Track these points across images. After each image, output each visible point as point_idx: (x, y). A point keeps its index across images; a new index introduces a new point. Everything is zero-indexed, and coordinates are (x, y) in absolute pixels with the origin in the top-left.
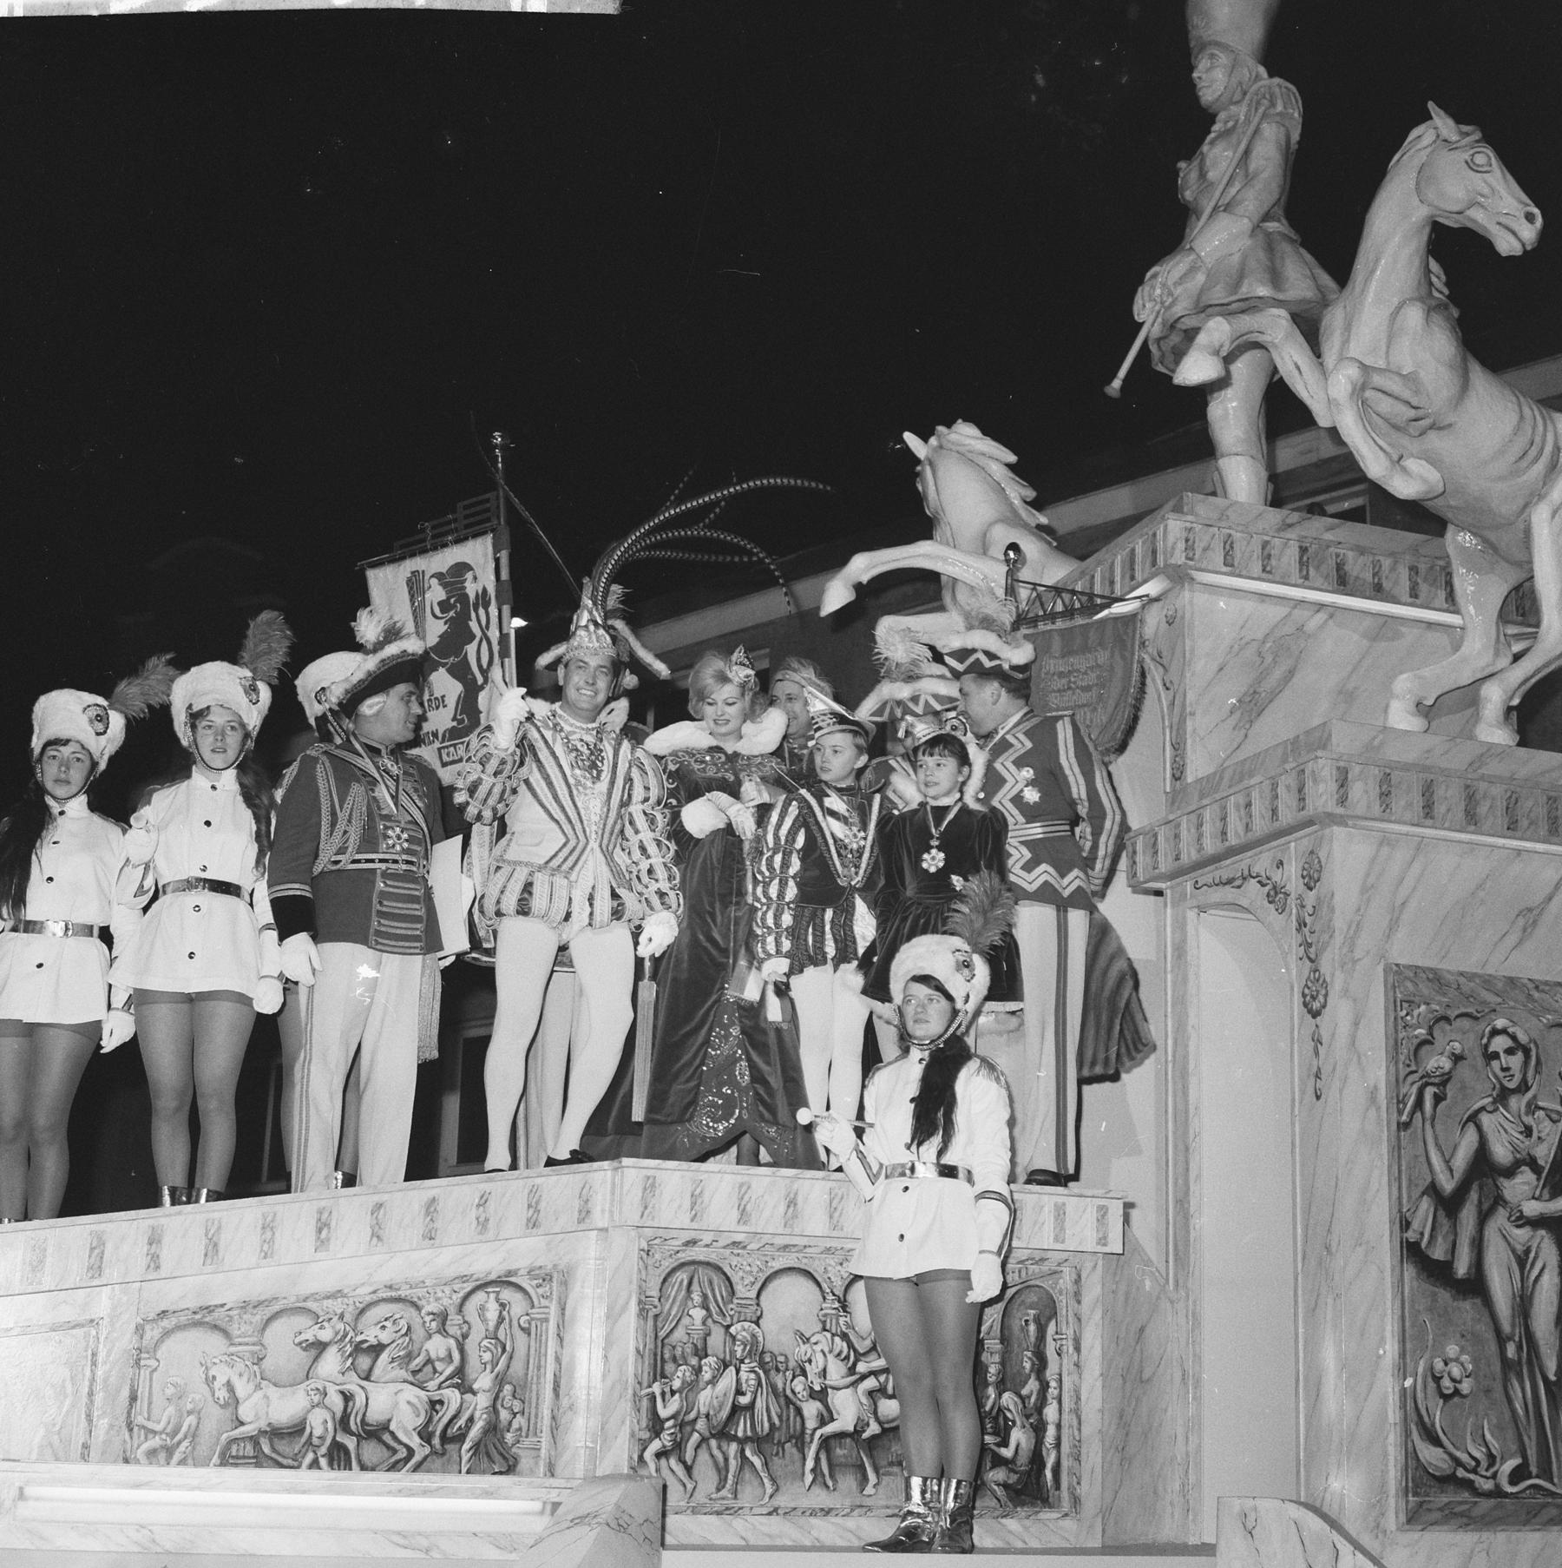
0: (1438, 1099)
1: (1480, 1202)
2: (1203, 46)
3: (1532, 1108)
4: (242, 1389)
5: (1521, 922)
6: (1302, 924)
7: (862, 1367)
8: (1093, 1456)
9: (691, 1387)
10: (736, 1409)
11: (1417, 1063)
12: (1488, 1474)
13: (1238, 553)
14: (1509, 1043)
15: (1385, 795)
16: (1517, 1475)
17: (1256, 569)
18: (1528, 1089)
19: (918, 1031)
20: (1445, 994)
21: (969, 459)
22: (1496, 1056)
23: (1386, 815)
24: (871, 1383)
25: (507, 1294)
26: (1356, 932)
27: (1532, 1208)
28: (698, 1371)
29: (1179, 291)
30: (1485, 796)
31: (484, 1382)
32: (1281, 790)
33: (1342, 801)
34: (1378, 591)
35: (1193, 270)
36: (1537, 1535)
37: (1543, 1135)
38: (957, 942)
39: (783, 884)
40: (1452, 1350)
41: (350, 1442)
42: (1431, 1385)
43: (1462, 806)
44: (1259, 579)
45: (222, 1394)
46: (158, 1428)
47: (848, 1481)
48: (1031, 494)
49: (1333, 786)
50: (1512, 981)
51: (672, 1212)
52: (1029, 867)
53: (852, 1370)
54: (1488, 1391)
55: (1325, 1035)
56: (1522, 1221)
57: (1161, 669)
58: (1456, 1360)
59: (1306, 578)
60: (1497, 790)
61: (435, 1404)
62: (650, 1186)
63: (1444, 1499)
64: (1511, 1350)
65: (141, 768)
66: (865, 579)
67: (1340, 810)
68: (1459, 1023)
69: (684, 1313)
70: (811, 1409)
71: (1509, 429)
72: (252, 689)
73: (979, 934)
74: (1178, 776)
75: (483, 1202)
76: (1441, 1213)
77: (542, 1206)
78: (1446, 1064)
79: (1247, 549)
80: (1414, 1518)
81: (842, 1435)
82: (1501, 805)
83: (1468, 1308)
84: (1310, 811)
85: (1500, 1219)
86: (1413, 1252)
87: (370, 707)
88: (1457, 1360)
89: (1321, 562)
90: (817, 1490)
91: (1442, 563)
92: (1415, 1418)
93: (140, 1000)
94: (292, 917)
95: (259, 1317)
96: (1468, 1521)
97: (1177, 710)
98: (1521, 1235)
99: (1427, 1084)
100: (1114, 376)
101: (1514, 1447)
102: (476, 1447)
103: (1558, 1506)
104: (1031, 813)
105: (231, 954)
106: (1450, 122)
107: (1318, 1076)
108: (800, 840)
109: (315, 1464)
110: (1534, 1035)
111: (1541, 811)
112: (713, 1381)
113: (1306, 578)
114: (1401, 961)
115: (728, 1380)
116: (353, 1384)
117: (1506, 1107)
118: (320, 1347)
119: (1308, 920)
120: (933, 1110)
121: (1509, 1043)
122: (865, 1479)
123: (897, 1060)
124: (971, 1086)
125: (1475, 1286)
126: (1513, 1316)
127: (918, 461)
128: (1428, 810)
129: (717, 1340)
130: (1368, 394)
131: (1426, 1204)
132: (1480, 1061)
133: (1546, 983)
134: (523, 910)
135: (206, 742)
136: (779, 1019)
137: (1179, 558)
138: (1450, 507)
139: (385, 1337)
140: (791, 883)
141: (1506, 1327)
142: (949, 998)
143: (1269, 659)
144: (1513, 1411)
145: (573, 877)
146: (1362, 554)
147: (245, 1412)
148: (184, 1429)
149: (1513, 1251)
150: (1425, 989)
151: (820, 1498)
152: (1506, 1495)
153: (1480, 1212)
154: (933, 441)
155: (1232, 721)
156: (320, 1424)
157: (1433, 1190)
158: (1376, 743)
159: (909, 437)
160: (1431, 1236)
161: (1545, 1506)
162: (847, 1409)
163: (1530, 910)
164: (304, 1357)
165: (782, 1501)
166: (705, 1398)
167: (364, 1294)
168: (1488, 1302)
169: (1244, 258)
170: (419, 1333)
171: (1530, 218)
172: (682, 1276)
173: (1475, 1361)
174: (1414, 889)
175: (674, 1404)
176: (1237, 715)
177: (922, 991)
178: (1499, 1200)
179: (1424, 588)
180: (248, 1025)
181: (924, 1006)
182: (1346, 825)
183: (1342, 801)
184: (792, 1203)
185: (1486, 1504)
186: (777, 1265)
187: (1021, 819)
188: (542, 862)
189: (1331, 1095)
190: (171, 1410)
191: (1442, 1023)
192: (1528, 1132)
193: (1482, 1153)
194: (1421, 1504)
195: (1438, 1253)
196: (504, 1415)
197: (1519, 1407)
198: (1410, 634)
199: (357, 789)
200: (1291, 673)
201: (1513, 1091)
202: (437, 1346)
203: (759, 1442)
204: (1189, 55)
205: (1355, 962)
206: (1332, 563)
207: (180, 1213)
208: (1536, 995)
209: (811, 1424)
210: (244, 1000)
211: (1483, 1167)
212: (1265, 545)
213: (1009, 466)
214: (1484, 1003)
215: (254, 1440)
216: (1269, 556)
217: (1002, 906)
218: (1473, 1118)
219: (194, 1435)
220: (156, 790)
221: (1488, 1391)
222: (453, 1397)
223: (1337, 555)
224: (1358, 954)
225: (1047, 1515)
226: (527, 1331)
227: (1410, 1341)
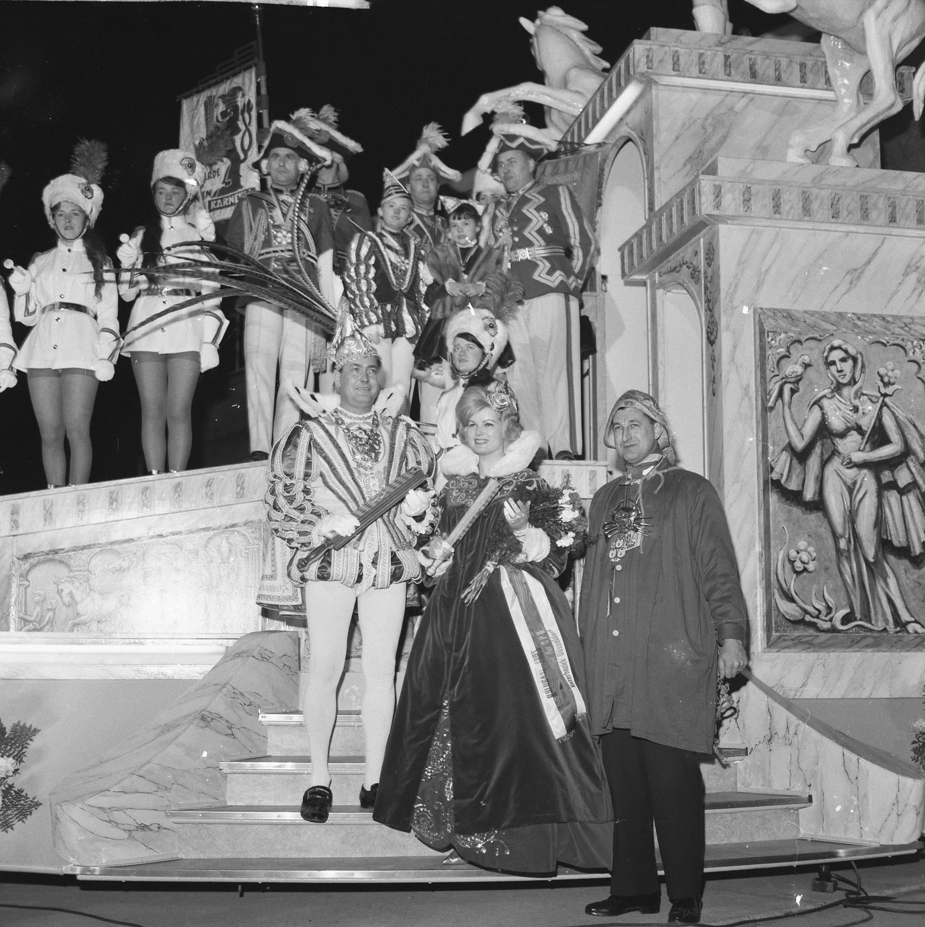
0: (793, 392)
1: (822, 454)
3: (859, 394)
5: (849, 278)
6: (706, 288)
11: (779, 370)
12: (827, 619)
14: (842, 354)
15: (747, 201)
16: (846, 619)
17: (695, 71)
18: (855, 383)
19: (462, 367)
20: (797, 326)
22: (834, 363)
23: (748, 214)
26: (734, 291)
27: (858, 457)
30: (816, 198)
33: (718, 206)
36: (859, 654)
37: (866, 411)
38: (486, 313)
40: (802, 544)
42: (788, 566)
43: (801, 204)
44: (698, 78)
45: (67, 599)
46: (32, 619)
48: (599, 49)
49: (712, 197)
50: (841, 315)
52: (550, 273)
54: (826, 569)
56: (851, 465)
58: (805, 550)
59: (729, 75)
63: (796, 634)
64: (843, 544)
67: (716, 212)
72: (87, 191)
74: (651, 209)
75: (209, 484)
76: (795, 461)
77: (245, 485)
78: (799, 369)
82: (827, 203)
83: (814, 518)
86: (773, 485)
88: (805, 551)
89: (740, 64)
91: (822, 59)
92: (777, 586)
96: (809, 645)
98: (851, 473)
99: (786, 382)
101: (845, 603)
103: (874, 637)
110: (861, 349)
111: (855, 205)
113: (729, 75)
114: (764, 306)
117: (840, 395)
121: (842, 354)
125: (819, 505)
126: (845, 524)
127: (529, 36)
128: (777, 208)
131: (785, 457)
132: (822, 367)
133: (864, 315)
138: (812, 18)
140: (373, 282)
141: (839, 529)
142: (480, 346)
143: (710, 130)
144: (844, 580)
146: (767, 57)
148: (47, 619)
149: (845, 483)
150: (783, 324)
152: (840, 631)
153: (822, 460)
154: (538, 22)
157: (790, 447)
158: (748, 170)
159: (524, 22)
160: (788, 476)
161: (865, 637)
163: (855, 270)
173: (818, 551)
174: (774, 261)
176: (688, 166)
177: (463, 342)
178: (835, 452)
179: (810, 77)
180: (94, 389)
182: (727, 223)
183: (718, 206)
185: (823, 637)
190: (38, 609)
191: (796, 344)
192: (856, 409)
194: (780, 637)
195: (793, 486)
200: (725, 138)
201: (845, 385)
206: (747, 64)
207: (28, 497)
208: (859, 323)
210: (91, 373)
211: (823, 431)
212: (701, 55)
213: (584, 33)
214: (824, 330)
216: (704, 63)
217: (512, 290)
220: (37, 256)
221: (826, 569)
223: (750, 59)
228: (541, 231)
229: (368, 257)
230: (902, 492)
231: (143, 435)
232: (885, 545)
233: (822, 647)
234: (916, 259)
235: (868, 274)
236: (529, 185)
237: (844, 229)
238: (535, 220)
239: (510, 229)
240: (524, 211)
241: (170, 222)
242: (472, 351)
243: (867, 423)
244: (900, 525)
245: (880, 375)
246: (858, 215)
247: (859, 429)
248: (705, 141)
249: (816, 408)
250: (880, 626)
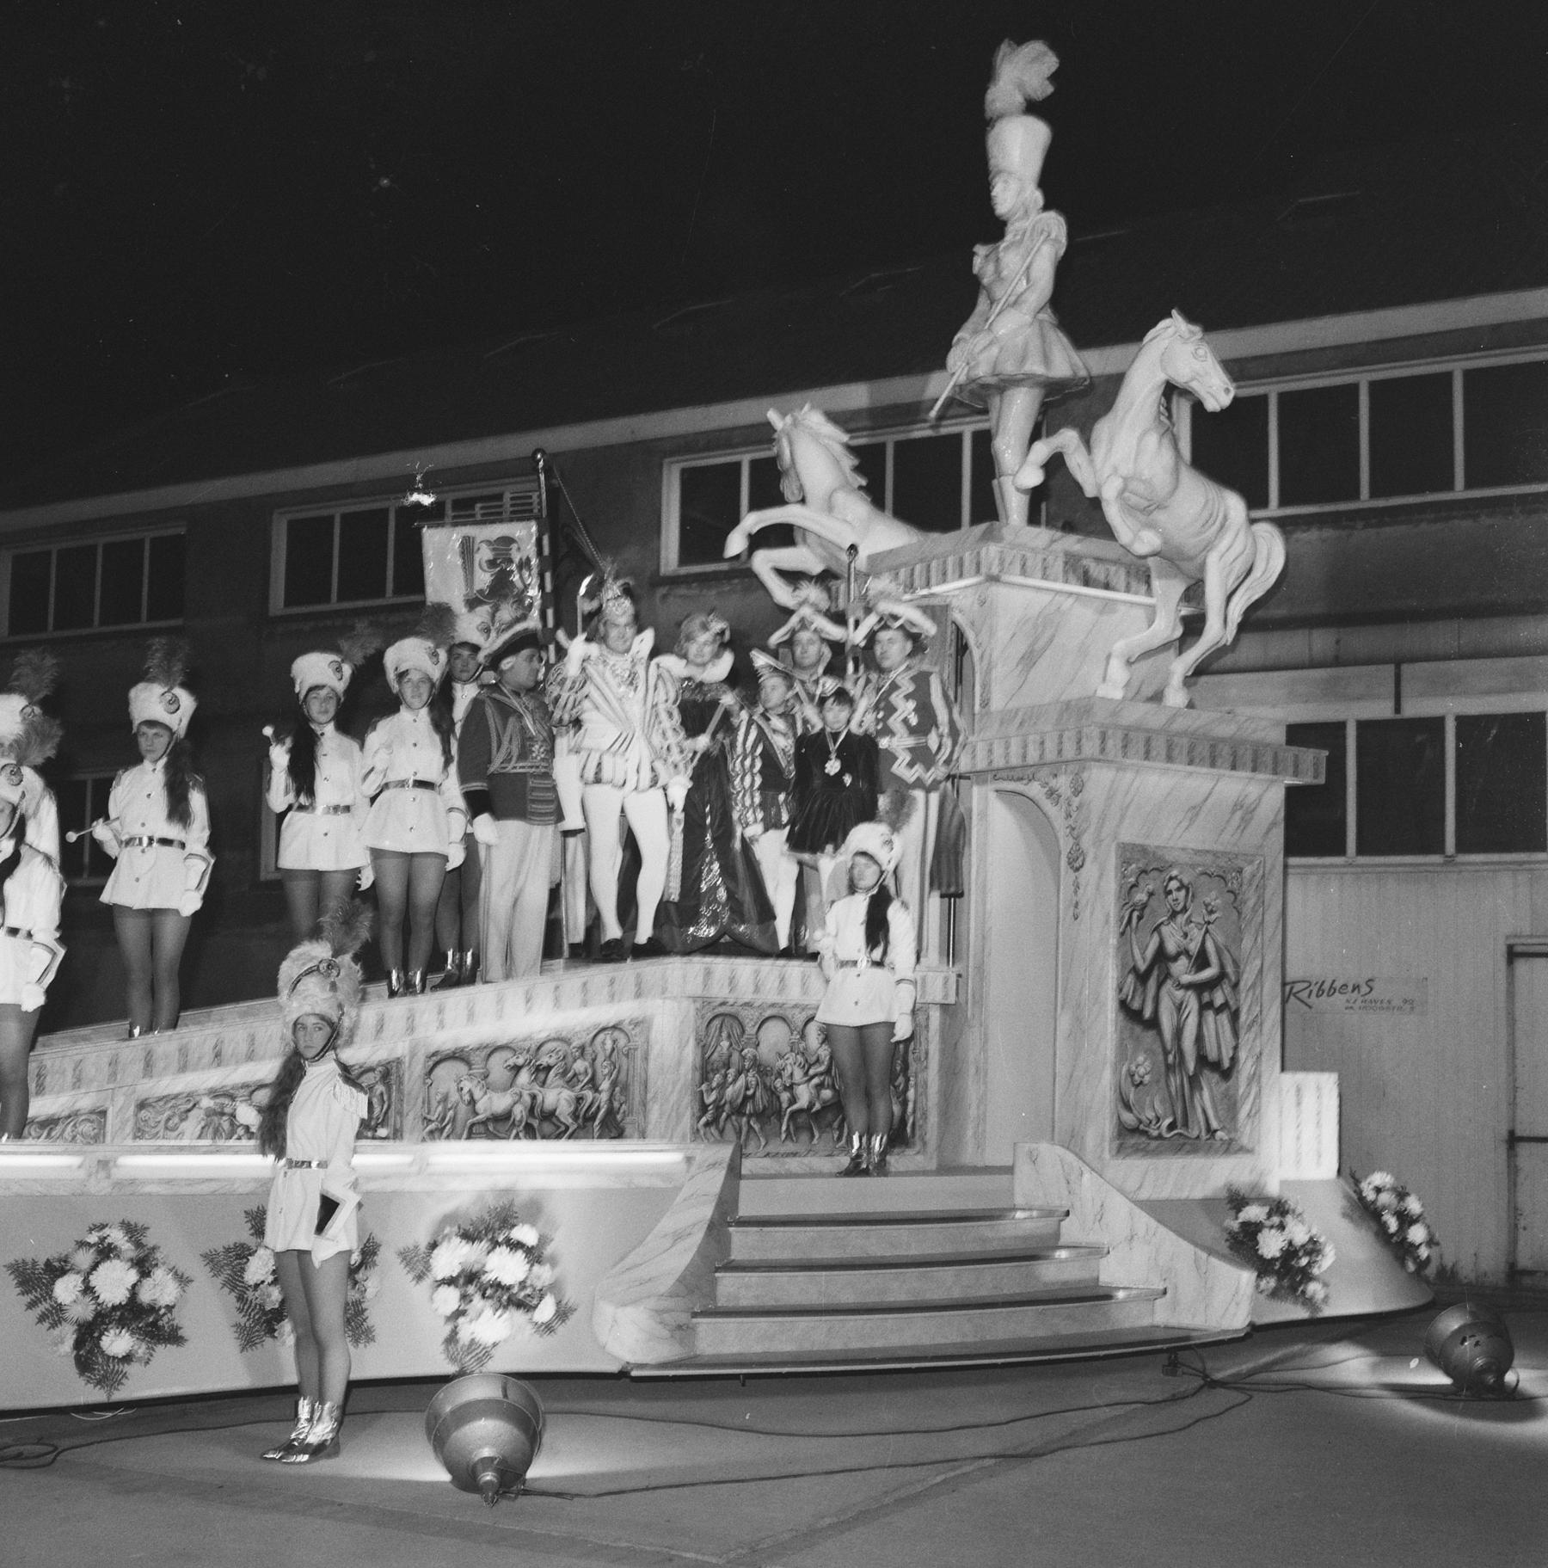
0: (1140, 918)
2: (999, 172)
3: (1189, 921)
4: (477, 1094)
6: (1069, 816)
7: (812, 1072)
8: (933, 1118)
9: (723, 1086)
10: (746, 1098)
13: (1029, 563)
16: (1172, 1127)
17: (1040, 574)
21: (816, 437)
22: (1170, 892)
24: (816, 1081)
25: (616, 1034)
28: (725, 1076)
31: (605, 1085)
32: (1065, 739)
34: (1107, 587)
35: (991, 343)
39: (753, 776)
41: (535, 1123)
47: (804, 1137)
49: (1098, 742)
51: (719, 991)
52: (911, 765)
53: (806, 1074)
55: (1082, 881)
56: (1180, 986)
60: (1185, 741)
61: (579, 1100)
62: (708, 973)
63: (1133, 1141)
64: (1171, 1058)
65: (366, 705)
66: (754, 531)
68: (1153, 874)
69: (718, 1044)
70: (785, 1096)
72: (435, 655)
75: (612, 982)
79: (1034, 562)
80: (1120, 1150)
81: (801, 1111)
83: (1151, 1034)
84: (1082, 756)
85: (1169, 985)
86: (1124, 1005)
87: (506, 664)
88: (1143, 1065)
90: (788, 1142)
93: (377, 854)
94: (477, 804)
95: (485, 1053)
97: (985, 661)
98: (1180, 994)
102: (603, 1122)
105: (430, 825)
108: (759, 749)
109: (517, 1137)
111: (1206, 753)
112: (735, 1081)
115: (741, 1081)
116: (536, 1089)
118: (517, 1069)
120: (877, 929)
122: (813, 1136)
124: (895, 914)
125: (1154, 1024)
129: (735, 1057)
130: (1127, 494)
131: (1131, 979)
135: (408, 692)
137: (995, 571)
139: (552, 1061)
141: (1169, 1046)
142: (876, 862)
147: (480, 1106)
151: (790, 1147)
154: (789, 419)
155: (1017, 672)
156: (519, 1112)
157: (1134, 969)
162: (804, 1095)
164: (508, 1074)
165: (771, 1148)
166: (730, 1091)
167: (543, 1036)
168: (1160, 1033)
169: (1026, 344)
170: (570, 1059)
171: (1227, 391)
172: (717, 1022)
175: (713, 1096)
177: (862, 860)
178: (1168, 975)
179: (1134, 584)
183: (1103, 750)
184: (782, 980)
185: (1154, 1144)
186: (767, 1014)
189: (1085, 915)
192: (1186, 935)
193: (1161, 948)
195: (1136, 1005)
196: (616, 1104)
197: (1173, 1089)
198: (1122, 608)
199: (512, 720)
202: (580, 1066)
203: (760, 1115)
209: (785, 1105)
211: (1162, 957)
215: (484, 1123)
218: (1157, 929)
219: (454, 1119)
222: (589, 1095)
225: (910, 1152)
226: (627, 1056)
227: (1122, 1054)
228: (905, 721)
229: (754, 747)
230: (1218, 1011)
232: (1202, 1059)
233: (1156, 1153)
235: (1204, 809)
243: (1194, 948)
244: (1213, 1039)
246: (1208, 761)
247: (1186, 952)
248: (1037, 639)
249: (1156, 935)
250: (1195, 1133)
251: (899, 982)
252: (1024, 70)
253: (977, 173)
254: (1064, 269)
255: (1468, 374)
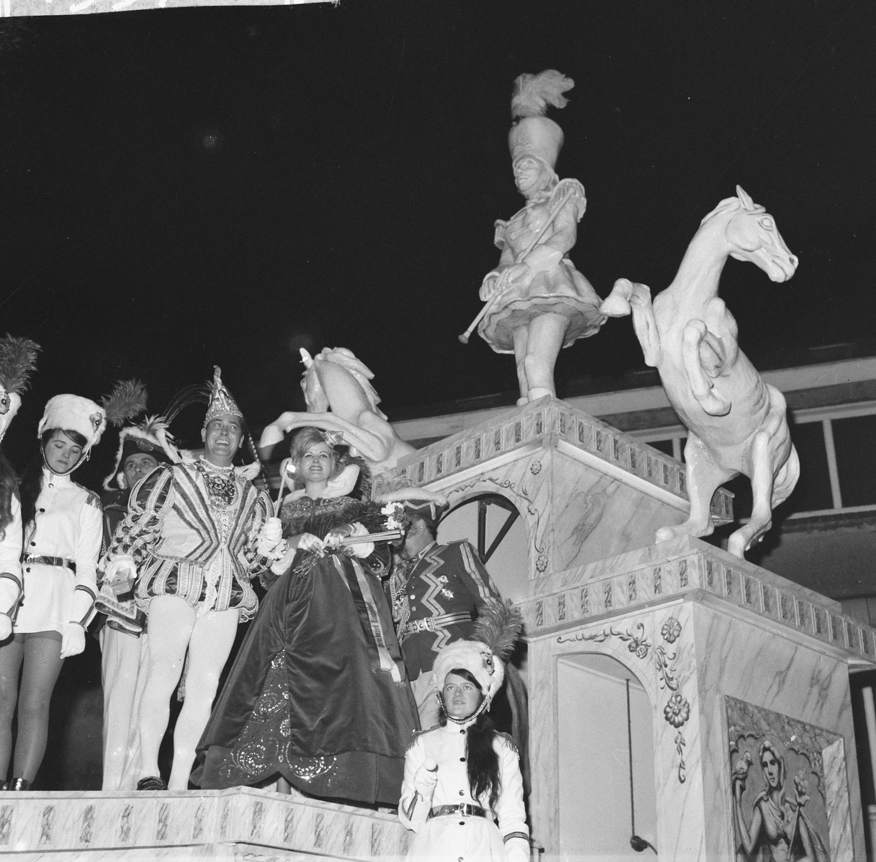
0: (743, 789)
3: (784, 801)
5: (777, 679)
6: (663, 665)
13: (586, 432)
18: (781, 788)
29: (514, 286)
38: (482, 646)
50: (778, 716)
57: (526, 503)
71: (753, 385)
73: (497, 640)
75: (127, 814)
77: (169, 822)
99: (737, 779)
100: (466, 329)
104: (448, 606)
106: (750, 199)
107: (682, 766)
110: (783, 755)
119: (668, 662)
123: (433, 729)
132: (760, 767)
133: (793, 720)
134: (171, 590)
136: (400, 680)
142: (479, 686)
143: (590, 505)
145: (206, 567)
154: (319, 357)
159: (303, 352)
177: (459, 681)
181: (461, 692)
184: (349, 833)
187: (442, 611)
188: (184, 556)
192: (782, 816)
204: (510, 161)
205: (706, 691)
208: (787, 727)
218: (758, 804)
224: (707, 687)
228: (440, 598)
231: (46, 744)
234: (816, 674)
236: (428, 548)
237: (774, 631)
238: (433, 586)
239: (407, 598)
240: (422, 577)
241: (51, 479)
242: (468, 691)
243: (790, 831)
245: (796, 784)
251: (507, 838)
252: (539, 92)
253: (502, 161)
254: (583, 227)
255: (835, 423)
